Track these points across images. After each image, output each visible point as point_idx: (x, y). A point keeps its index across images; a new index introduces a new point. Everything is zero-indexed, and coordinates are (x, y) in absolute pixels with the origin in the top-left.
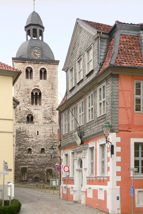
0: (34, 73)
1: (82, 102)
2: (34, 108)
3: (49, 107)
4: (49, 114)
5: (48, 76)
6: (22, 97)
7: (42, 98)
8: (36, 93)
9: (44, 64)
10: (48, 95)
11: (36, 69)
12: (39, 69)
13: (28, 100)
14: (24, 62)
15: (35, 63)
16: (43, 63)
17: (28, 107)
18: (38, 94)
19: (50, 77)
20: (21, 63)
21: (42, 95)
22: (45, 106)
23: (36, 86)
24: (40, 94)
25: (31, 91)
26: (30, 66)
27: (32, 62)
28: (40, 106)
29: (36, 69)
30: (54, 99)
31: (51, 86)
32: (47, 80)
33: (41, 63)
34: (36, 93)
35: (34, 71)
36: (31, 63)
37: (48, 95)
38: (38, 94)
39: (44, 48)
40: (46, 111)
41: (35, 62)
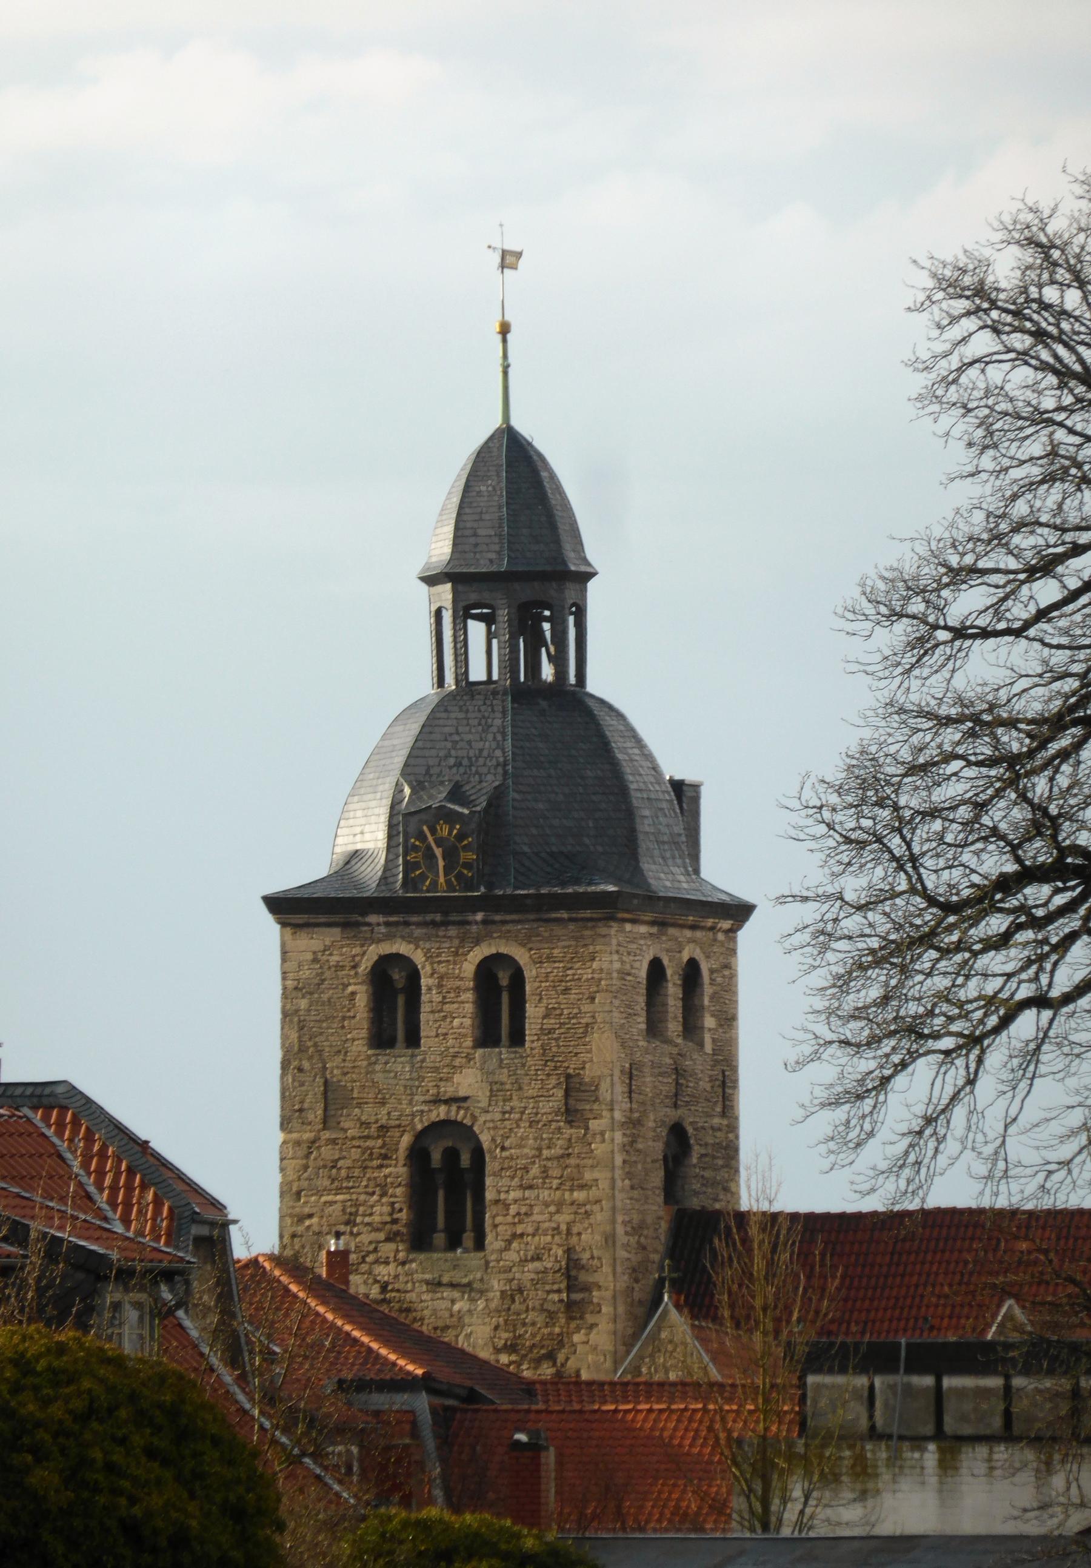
0: (429, 998)
1: (753, 1297)
2: (427, 1276)
3: (537, 1265)
4: (540, 1319)
5: (533, 1011)
6: (339, 1191)
7: (489, 1195)
8: (451, 1155)
9: (504, 922)
10: (535, 1170)
11: (442, 968)
12: (469, 968)
13: (380, 1212)
14: (358, 924)
15: (434, 924)
16: (498, 918)
17: (384, 1272)
18: (465, 1160)
19: (550, 1022)
20: (337, 931)
21: (491, 1166)
22: (512, 1256)
23: (1037, 1125)
24: (478, 1154)
25: (406, 1140)
26: (402, 948)
27: (415, 919)
28: (474, 1259)
29: (442, 968)
30: (579, 1195)
31: (560, 1093)
32: (527, 1045)
33: (479, 916)
34: (451, 1155)
35: (431, 981)
36: (407, 924)
37: (535, 1170)
38: (465, 1160)
39: (936, 1144)
40: (520, 1290)
41: (438, 917)
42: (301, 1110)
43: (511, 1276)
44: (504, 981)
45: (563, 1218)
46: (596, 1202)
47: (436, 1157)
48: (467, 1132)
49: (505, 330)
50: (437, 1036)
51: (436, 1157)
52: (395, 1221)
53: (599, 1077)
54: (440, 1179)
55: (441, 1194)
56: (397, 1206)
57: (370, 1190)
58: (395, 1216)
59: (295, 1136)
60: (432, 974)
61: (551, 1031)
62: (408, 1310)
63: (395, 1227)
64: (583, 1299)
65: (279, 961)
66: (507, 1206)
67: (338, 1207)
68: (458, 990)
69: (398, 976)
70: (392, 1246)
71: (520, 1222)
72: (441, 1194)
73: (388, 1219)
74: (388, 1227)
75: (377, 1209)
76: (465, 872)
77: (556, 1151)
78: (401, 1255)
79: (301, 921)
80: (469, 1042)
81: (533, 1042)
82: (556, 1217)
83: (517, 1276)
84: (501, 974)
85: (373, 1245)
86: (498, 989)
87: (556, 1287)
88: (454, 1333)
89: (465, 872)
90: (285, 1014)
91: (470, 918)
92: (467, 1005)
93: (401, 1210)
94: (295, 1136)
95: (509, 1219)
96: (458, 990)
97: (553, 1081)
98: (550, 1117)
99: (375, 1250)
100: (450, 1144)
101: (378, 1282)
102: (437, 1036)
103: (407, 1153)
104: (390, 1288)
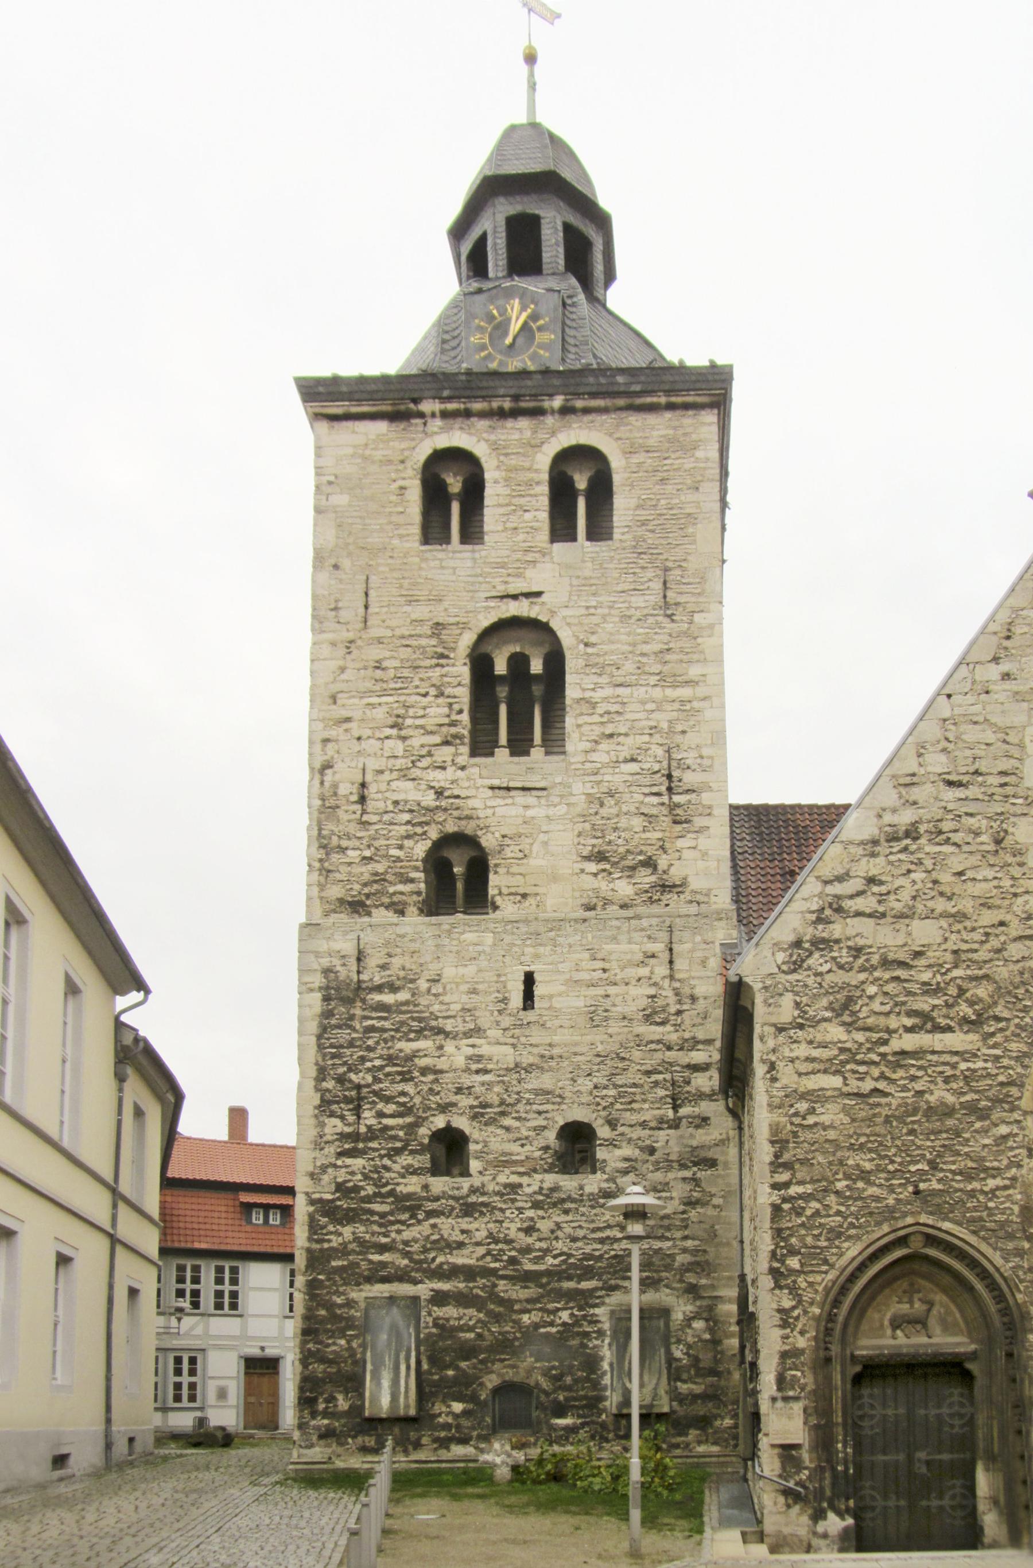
3: (633, 767)
12: (544, 460)
13: (437, 712)
18: (536, 666)
21: (572, 664)
22: (601, 757)
24: (556, 661)
25: (468, 639)
27: (477, 406)
30: (685, 692)
34: (518, 662)
36: (467, 414)
37: (629, 667)
42: (336, 609)
43: (599, 778)
44: (581, 482)
45: (662, 719)
46: (704, 699)
47: (501, 668)
48: (540, 628)
49: (531, 59)
50: (505, 529)
51: (501, 668)
52: (453, 724)
53: (564, 753)
54: (502, 692)
55: (503, 709)
56: (456, 707)
57: (423, 691)
58: (454, 717)
59: (329, 636)
60: (498, 467)
61: (643, 523)
62: (469, 818)
63: (453, 730)
64: (690, 801)
65: (312, 456)
66: (594, 705)
67: (385, 709)
68: (529, 484)
69: (454, 484)
70: (449, 750)
71: (610, 722)
72: (503, 709)
73: (446, 721)
74: (445, 729)
75: (431, 711)
76: (542, 352)
77: (656, 647)
78: (462, 760)
79: (339, 411)
80: (544, 534)
81: (623, 534)
82: (655, 716)
83: (607, 778)
84: (577, 477)
85: (427, 749)
86: (573, 494)
87: (655, 789)
88: (529, 841)
89: (542, 352)
90: (318, 510)
91: (546, 404)
92: (541, 498)
93: (460, 712)
94: (329, 636)
95: (596, 719)
96: (529, 484)
97: (650, 574)
98: (646, 611)
99: (430, 754)
100: (518, 650)
101: (433, 788)
102: (505, 529)
103: (468, 651)
104: (446, 794)
